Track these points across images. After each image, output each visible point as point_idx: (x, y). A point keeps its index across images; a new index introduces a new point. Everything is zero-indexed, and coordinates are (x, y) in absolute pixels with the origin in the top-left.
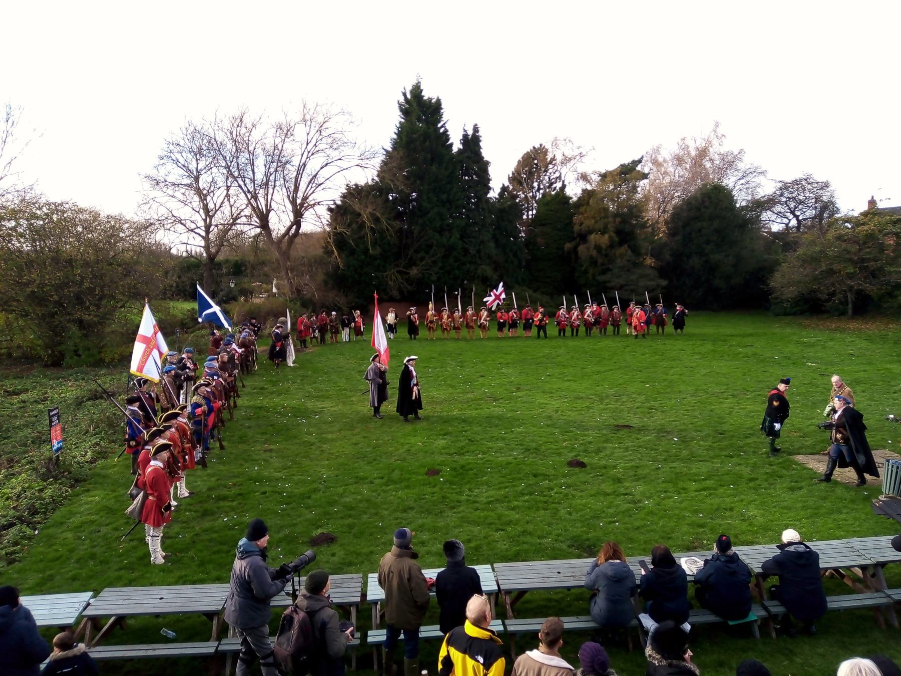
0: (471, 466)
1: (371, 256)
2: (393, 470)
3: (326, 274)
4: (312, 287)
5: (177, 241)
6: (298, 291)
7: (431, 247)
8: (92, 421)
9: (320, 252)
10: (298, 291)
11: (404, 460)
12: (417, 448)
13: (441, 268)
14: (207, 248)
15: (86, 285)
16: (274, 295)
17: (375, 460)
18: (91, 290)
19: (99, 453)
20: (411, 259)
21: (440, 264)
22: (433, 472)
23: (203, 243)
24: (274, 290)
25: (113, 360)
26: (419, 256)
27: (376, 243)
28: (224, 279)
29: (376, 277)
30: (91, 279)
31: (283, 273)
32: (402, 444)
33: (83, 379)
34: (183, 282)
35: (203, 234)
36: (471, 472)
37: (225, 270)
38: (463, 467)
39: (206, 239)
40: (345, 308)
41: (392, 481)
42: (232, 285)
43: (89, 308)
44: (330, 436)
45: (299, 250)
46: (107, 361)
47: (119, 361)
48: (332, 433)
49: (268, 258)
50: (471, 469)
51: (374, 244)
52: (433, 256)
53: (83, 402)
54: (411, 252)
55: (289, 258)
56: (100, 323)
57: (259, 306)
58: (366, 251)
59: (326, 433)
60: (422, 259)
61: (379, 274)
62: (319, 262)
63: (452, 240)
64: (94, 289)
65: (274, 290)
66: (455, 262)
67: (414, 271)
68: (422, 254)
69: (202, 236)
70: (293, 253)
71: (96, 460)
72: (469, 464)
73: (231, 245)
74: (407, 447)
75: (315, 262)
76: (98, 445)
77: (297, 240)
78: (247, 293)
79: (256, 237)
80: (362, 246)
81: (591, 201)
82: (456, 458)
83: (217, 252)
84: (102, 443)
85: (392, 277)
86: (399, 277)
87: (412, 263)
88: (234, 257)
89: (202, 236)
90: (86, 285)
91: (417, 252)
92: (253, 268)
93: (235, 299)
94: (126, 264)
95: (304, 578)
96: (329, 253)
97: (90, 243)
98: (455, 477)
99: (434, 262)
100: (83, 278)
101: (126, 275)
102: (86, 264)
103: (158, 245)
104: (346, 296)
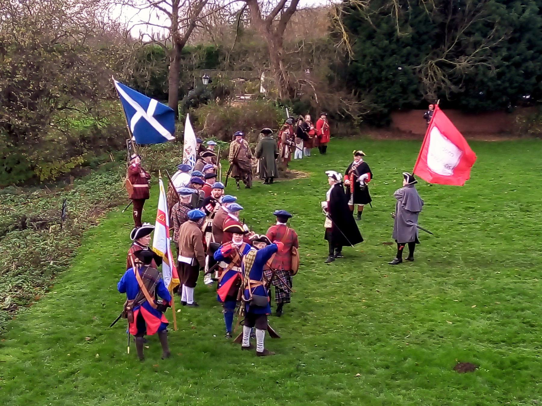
0: (526, 363)
1: (398, 40)
2: (405, 359)
3: (332, 67)
4: (311, 80)
5: (136, 20)
6: (291, 91)
7: (490, 26)
8: (15, 256)
9: (325, 35)
10: (291, 91)
11: (423, 344)
12: (444, 328)
13: (505, 59)
14: (174, 29)
15: (19, 77)
16: (260, 97)
17: (379, 340)
18: (24, 85)
19: (20, 299)
20: (459, 44)
21: (504, 53)
22: (467, 367)
23: (169, 23)
24: (262, 90)
25: (50, 179)
26: (472, 39)
27: (406, 21)
28: (195, 73)
29: (405, 73)
30: (25, 69)
31: (272, 67)
32: (422, 321)
33: (12, 201)
34: (142, 76)
35: (170, 9)
36: (524, 372)
37: (195, 62)
38: (513, 363)
39: (174, 17)
40: (355, 117)
41: (402, 373)
42: (205, 82)
43: (20, 108)
44: (318, 300)
45: (296, 33)
46: (42, 179)
47: (58, 179)
48: (321, 296)
49: (252, 43)
50: (526, 368)
51: (404, 23)
52: (494, 40)
53: (8, 231)
54: (459, 34)
55: (281, 45)
56: (33, 129)
57: (236, 113)
58: (390, 34)
59: (314, 295)
60: (476, 44)
61: (407, 67)
62: (323, 49)
63: (527, 14)
64: (28, 83)
65: (262, 90)
66: (529, 48)
67: (462, 64)
68: (477, 37)
69: (168, 13)
70: (287, 38)
71: (15, 308)
72: (524, 359)
73: (205, 25)
74: (428, 325)
75: (318, 48)
76: (20, 288)
77: (295, 18)
78: (224, 93)
79: (239, 14)
80: (384, 26)
81: (244, 259)
82: (504, 349)
83: (187, 36)
84: (25, 286)
85: (429, 73)
86: (439, 72)
87: (460, 51)
88: (207, 44)
89: (168, 13)
90: (19, 77)
91: (468, 34)
92: (233, 58)
93: (205, 101)
94: (68, 51)
95: (361, 160)
96: (336, 36)
97: (29, 23)
98: (500, 377)
99: (495, 49)
100: (15, 68)
101: (68, 67)
102: (20, 50)
103: (115, 26)
104: (359, 99)
